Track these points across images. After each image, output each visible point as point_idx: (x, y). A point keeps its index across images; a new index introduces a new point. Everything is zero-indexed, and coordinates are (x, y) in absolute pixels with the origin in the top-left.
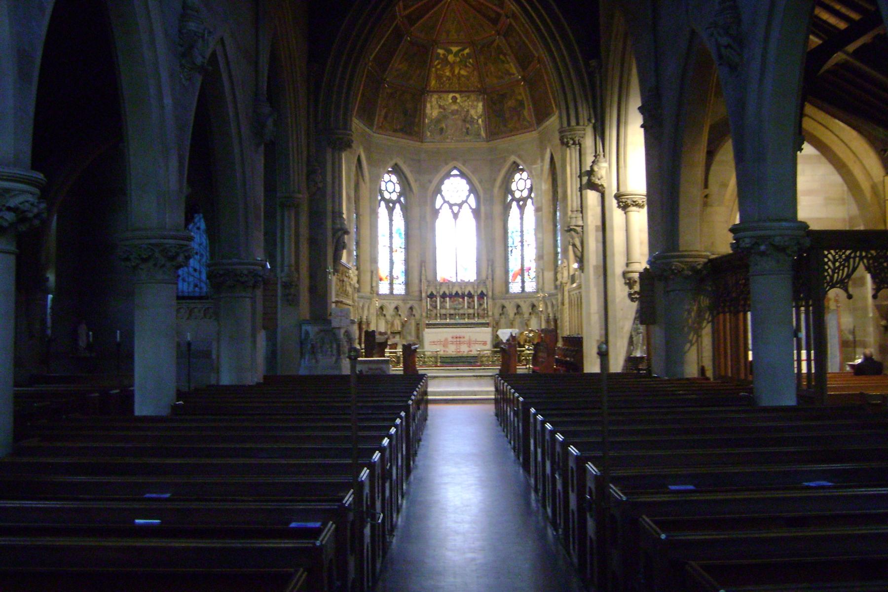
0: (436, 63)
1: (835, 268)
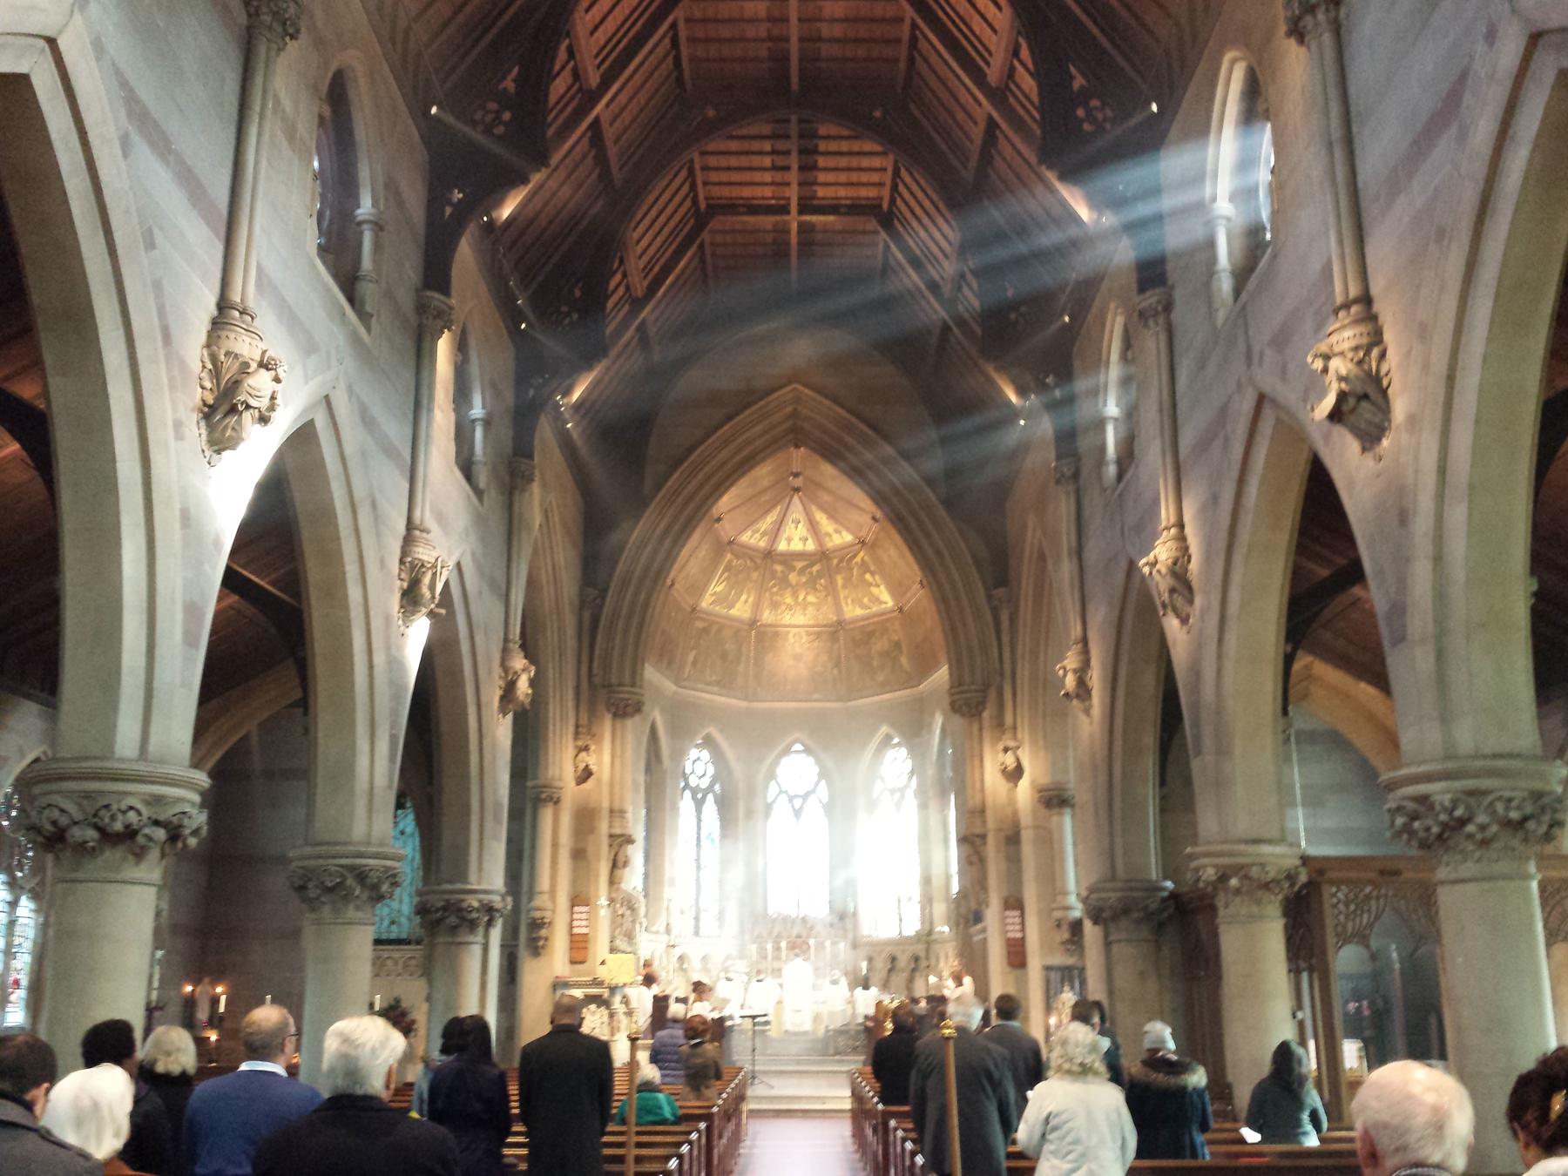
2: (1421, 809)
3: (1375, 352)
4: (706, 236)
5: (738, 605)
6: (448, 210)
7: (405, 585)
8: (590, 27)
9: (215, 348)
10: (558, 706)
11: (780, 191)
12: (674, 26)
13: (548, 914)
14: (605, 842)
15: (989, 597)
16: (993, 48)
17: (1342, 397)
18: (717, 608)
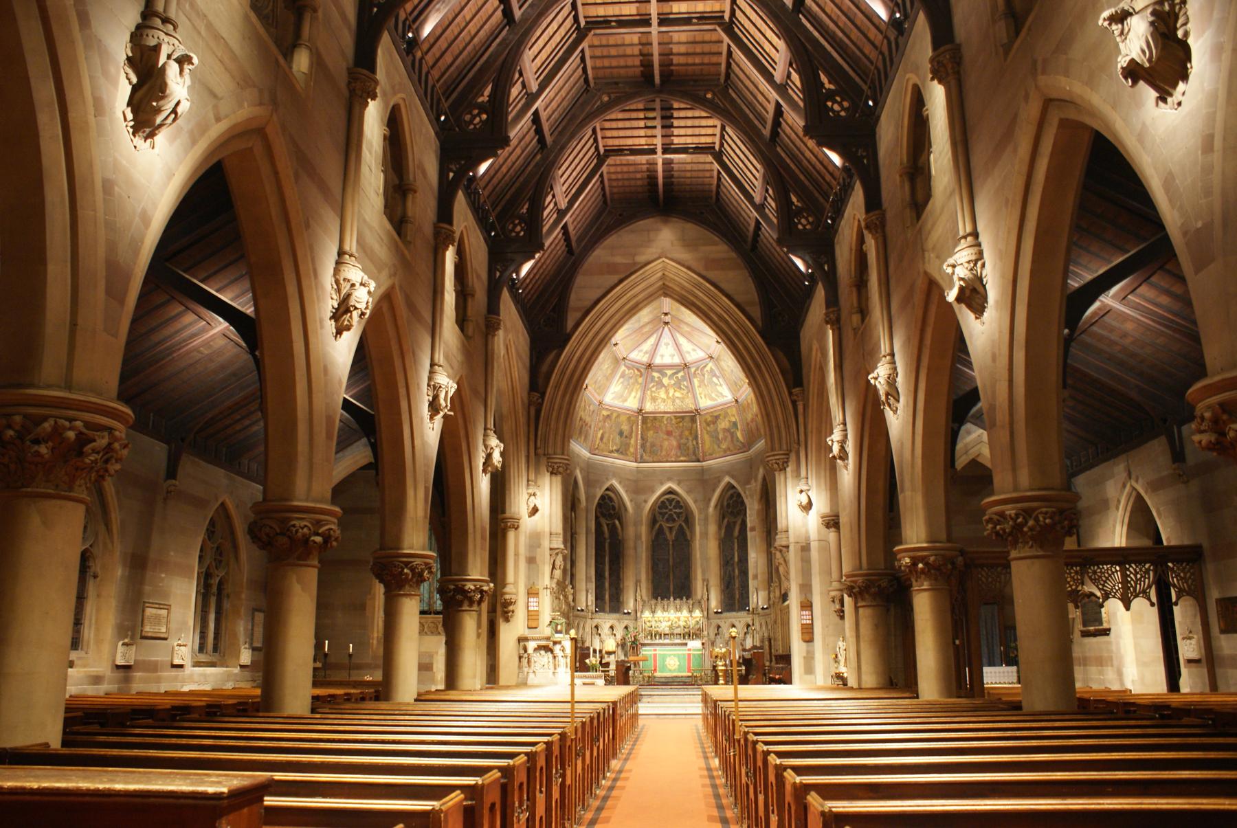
0: (651, 385)
1: (1137, 580)
2: (1002, 520)
3: (979, 264)
4: (604, 169)
6: (451, 175)
7: (431, 399)
8: (532, 57)
9: (337, 277)
10: (516, 467)
11: (650, 141)
12: (582, 51)
13: (513, 597)
14: (547, 552)
15: (790, 394)
16: (777, 61)
17: (961, 289)
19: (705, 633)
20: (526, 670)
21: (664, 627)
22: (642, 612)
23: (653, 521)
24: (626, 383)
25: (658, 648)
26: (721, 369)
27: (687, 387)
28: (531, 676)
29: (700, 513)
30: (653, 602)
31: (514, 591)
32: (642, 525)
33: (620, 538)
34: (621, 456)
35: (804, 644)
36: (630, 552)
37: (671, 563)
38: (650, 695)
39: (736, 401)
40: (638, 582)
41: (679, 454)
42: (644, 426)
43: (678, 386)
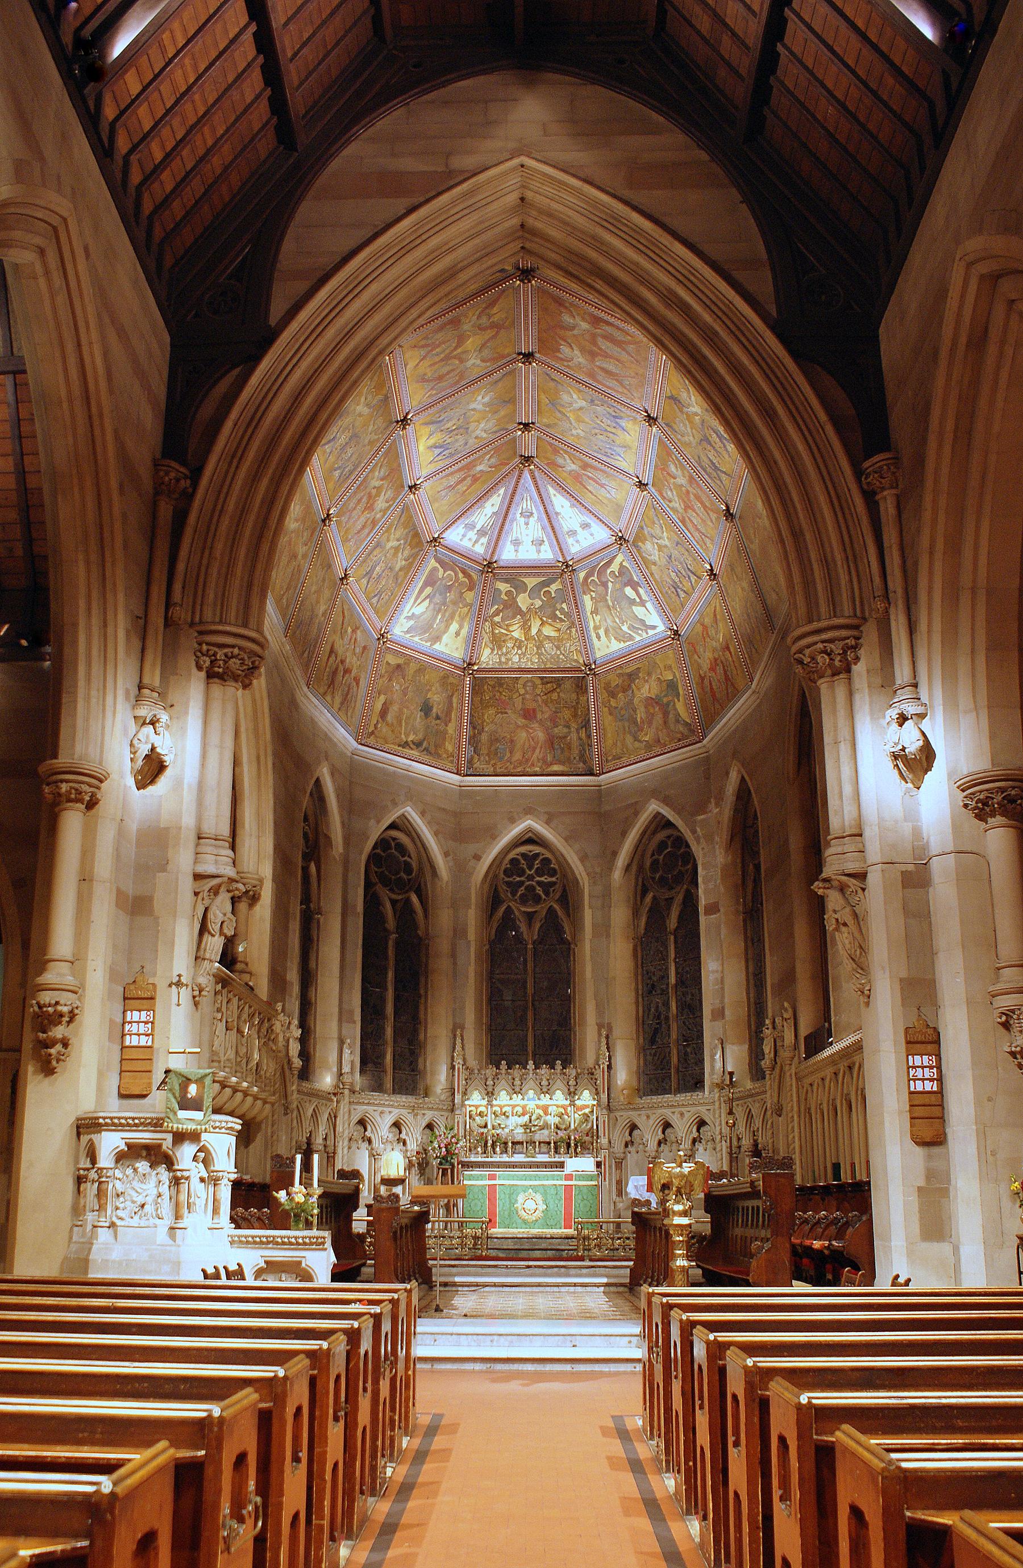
5: (445, 638)
10: (95, 621)
14: (187, 885)
15: (859, 473)
18: (416, 639)
19: (604, 1141)
20: (90, 1217)
21: (513, 1126)
22: (465, 1094)
23: (493, 901)
24: (438, 599)
25: (499, 1172)
26: (644, 563)
27: (568, 615)
28: (104, 1235)
29: (594, 883)
30: (491, 1071)
31: (69, 980)
32: (469, 907)
33: (420, 933)
34: (426, 758)
35: (919, 1151)
36: (441, 964)
37: (530, 990)
38: (477, 1285)
39: (676, 633)
40: (457, 1028)
41: (549, 759)
42: (477, 699)
43: (549, 613)
